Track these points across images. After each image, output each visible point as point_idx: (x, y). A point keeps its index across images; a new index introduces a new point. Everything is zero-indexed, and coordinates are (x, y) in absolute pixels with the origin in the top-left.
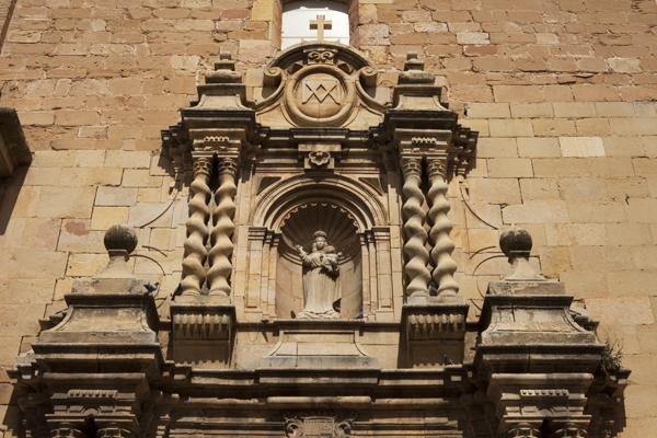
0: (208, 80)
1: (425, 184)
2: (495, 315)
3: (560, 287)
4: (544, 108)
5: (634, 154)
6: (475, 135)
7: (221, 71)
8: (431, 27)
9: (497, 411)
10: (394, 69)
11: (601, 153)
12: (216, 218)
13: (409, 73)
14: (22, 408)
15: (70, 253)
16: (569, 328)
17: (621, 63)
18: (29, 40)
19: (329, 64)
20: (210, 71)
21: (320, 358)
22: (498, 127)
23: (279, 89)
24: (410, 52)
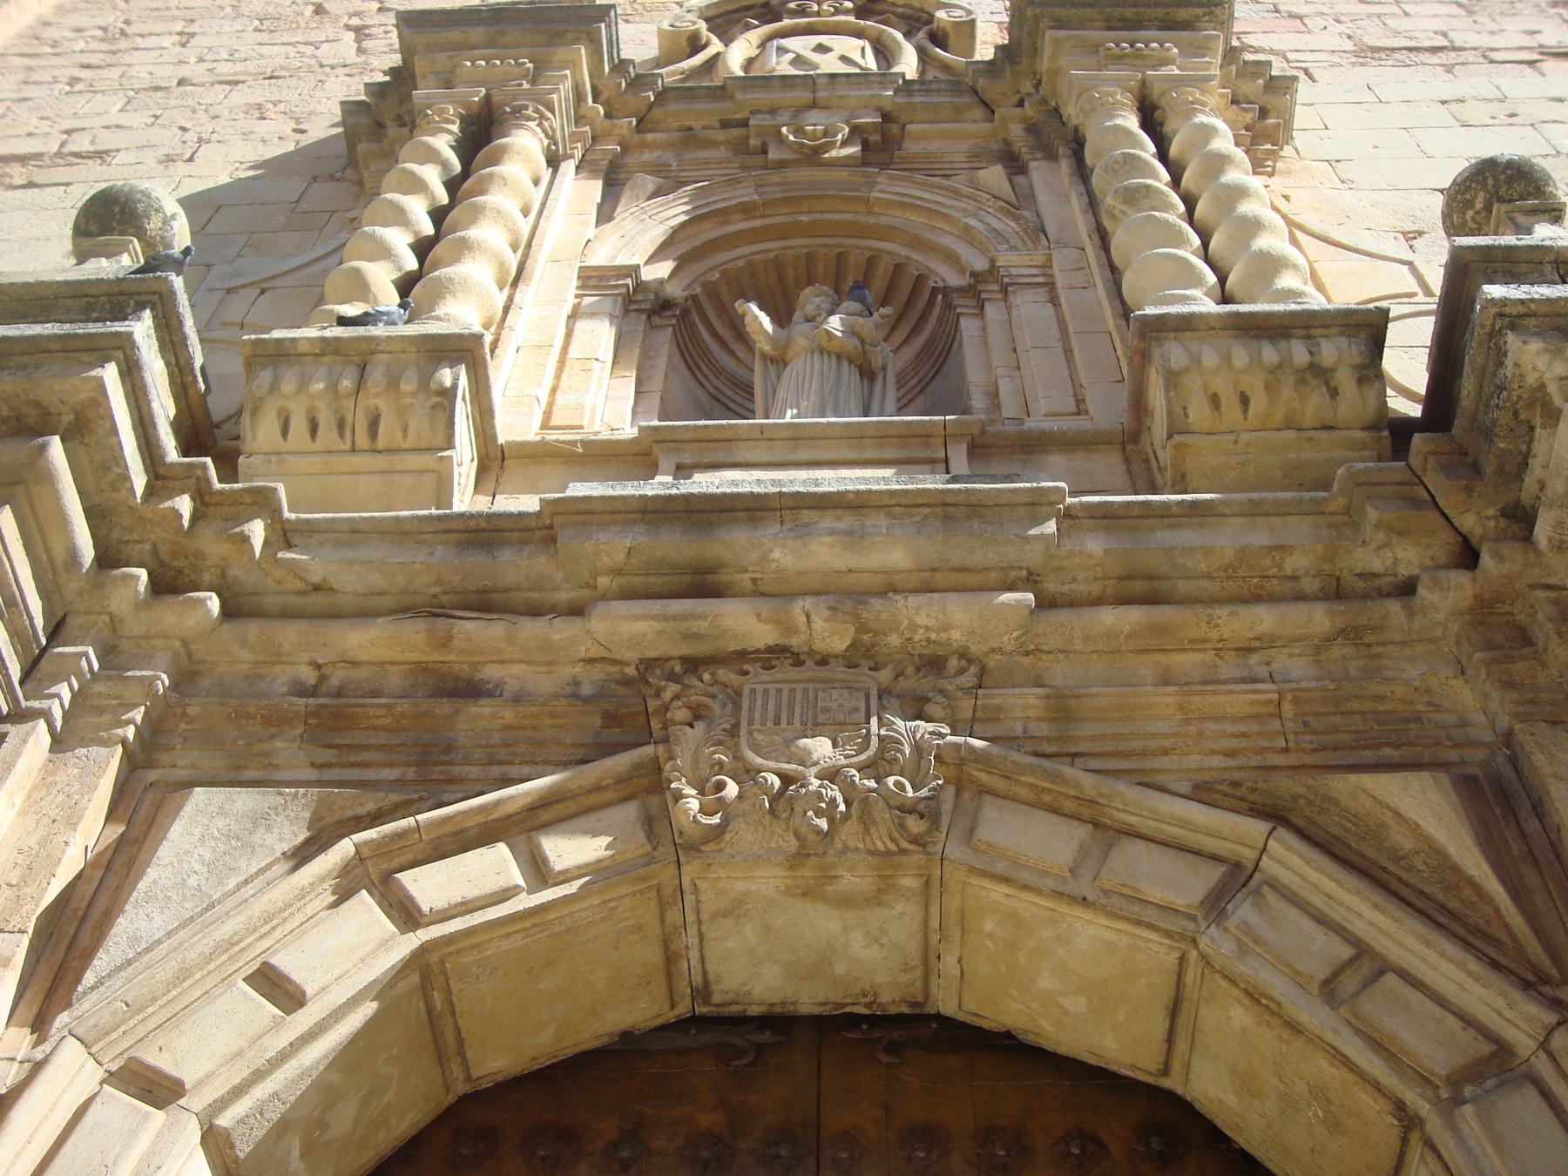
12: (166, 585)
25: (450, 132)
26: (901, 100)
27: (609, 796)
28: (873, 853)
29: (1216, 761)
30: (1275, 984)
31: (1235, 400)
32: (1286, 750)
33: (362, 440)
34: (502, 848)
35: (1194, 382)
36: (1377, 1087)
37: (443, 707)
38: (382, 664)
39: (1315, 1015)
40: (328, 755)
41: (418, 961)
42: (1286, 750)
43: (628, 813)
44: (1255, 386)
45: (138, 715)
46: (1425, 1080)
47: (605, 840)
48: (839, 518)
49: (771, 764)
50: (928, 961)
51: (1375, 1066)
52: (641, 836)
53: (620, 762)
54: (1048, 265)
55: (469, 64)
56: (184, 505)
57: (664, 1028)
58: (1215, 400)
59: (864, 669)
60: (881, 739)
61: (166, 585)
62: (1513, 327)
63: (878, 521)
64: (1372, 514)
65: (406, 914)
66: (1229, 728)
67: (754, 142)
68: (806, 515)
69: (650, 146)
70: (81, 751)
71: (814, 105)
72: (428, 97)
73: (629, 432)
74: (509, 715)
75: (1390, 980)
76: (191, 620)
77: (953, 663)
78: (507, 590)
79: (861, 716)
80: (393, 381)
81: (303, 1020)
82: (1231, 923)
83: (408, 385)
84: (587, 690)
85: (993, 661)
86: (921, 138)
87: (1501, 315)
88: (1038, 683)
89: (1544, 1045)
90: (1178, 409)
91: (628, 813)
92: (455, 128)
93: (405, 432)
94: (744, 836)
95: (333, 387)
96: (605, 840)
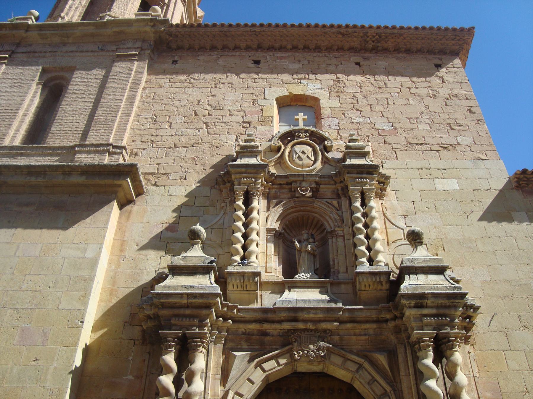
0: (242, 147)
1: (363, 204)
2: (407, 277)
3: (441, 260)
4: (425, 164)
5: (475, 188)
6: (387, 178)
7: (248, 144)
8: (361, 120)
9: (409, 329)
10: (342, 142)
11: (457, 187)
12: (225, 319)
13: (351, 144)
14: (144, 328)
15: (167, 243)
16: (448, 283)
17: (465, 140)
18: (142, 127)
19: (307, 140)
20: (242, 143)
21: (309, 301)
22: (400, 173)
23: (280, 153)
24: (351, 133)
25: (242, 199)
26: (320, 180)
27: (285, 352)
28: (318, 361)
29: (360, 347)
30: (363, 382)
31: (368, 286)
32: (369, 345)
33: (245, 289)
34: (274, 361)
35: (363, 284)
36: (373, 395)
37: (263, 337)
38: (253, 329)
39: (367, 386)
40: (249, 344)
41: (267, 377)
42: (369, 345)
43: (288, 355)
44: (371, 284)
45: (224, 339)
46: (377, 395)
47: (286, 360)
48: (314, 311)
49: (306, 349)
50: (323, 369)
51: (372, 393)
52: (290, 359)
53: (286, 348)
54: (343, 231)
55: (243, 179)
56: (226, 309)
57: (291, 374)
58: (365, 286)
59: (316, 333)
60: (319, 345)
61: (225, 319)
62: (403, 297)
63: (319, 311)
64: (383, 312)
65: (264, 370)
66: (362, 342)
67: (293, 190)
68: (309, 310)
69: (274, 188)
70: (218, 345)
71: (304, 181)
72: (237, 188)
73: (280, 280)
74: (271, 338)
75: (376, 382)
76: (228, 325)
77: (328, 331)
78: (269, 318)
79: (316, 341)
80: (249, 280)
81: (255, 385)
82: (359, 373)
83: (251, 281)
84: (281, 334)
85: (333, 330)
86: (324, 189)
87: (401, 295)
88: (339, 335)
89: (390, 392)
90: (360, 288)
91: (288, 355)
92: (242, 197)
93: (251, 288)
94: (303, 359)
95: (240, 281)
96: (286, 360)
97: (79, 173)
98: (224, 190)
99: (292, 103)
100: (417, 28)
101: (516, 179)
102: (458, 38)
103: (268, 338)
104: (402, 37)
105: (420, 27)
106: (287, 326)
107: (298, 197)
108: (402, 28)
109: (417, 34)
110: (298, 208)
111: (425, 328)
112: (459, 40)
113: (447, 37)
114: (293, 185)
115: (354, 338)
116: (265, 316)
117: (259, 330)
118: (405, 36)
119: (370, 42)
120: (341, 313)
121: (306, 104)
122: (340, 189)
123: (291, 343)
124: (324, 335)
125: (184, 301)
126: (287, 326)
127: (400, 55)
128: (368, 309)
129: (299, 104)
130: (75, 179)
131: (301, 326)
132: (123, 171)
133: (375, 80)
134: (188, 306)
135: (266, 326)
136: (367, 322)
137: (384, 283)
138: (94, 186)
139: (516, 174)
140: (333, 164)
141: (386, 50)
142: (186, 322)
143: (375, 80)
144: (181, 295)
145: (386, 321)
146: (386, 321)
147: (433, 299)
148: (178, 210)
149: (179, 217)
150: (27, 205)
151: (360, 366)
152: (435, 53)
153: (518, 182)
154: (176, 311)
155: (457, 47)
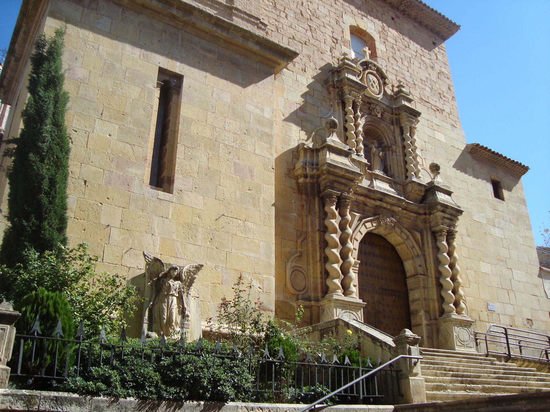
19: (375, 72)
39: (410, 249)
43: (376, 221)
51: (412, 253)
67: (371, 109)
97: (255, 41)
98: (332, 92)
99: (355, 33)
100: (432, 10)
101: (471, 148)
102: (450, 29)
103: (368, 208)
104: (422, 12)
105: (435, 10)
106: (378, 203)
107: (373, 115)
108: (425, 5)
109: (431, 14)
110: (371, 123)
111: (445, 225)
112: (449, 30)
113: (445, 25)
114: (372, 105)
115: (405, 219)
116: (368, 193)
117: (363, 201)
118: (424, 11)
119: (403, 5)
120: (404, 203)
121: (363, 38)
122: (394, 119)
123: (379, 214)
124: (393, 214)
125: (342, 173)
126: (378, 203)
127: (415, 24)
128: (415, 205)
129: (359, 35)
130: (251, 45)
131: (384, 205)
132: (287, 55)
133: (403, 39)
134: (342, 177)
135: (368, 200)
136: (411, 212)
137: (423, 192)
138: (261, 56)
139: (473, 144)
140: (388, 97)
141: (409, 16)
142: (342, 187)
143: (403, 39)
144: (342, 168)
145: (420, 214)
146: (420, 214)
147: (450, 210)
148: (304, 96)
149: (305, 102)
150: (210, 51)
151: (408, 238)
152: (433, 33)
153: (472, 149)
154: (337, 179)
155: (446, 35)
